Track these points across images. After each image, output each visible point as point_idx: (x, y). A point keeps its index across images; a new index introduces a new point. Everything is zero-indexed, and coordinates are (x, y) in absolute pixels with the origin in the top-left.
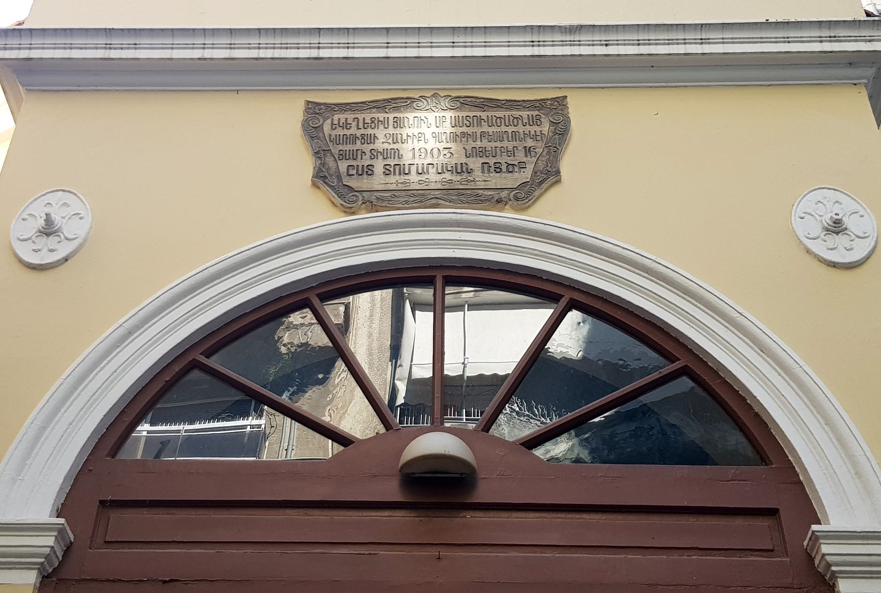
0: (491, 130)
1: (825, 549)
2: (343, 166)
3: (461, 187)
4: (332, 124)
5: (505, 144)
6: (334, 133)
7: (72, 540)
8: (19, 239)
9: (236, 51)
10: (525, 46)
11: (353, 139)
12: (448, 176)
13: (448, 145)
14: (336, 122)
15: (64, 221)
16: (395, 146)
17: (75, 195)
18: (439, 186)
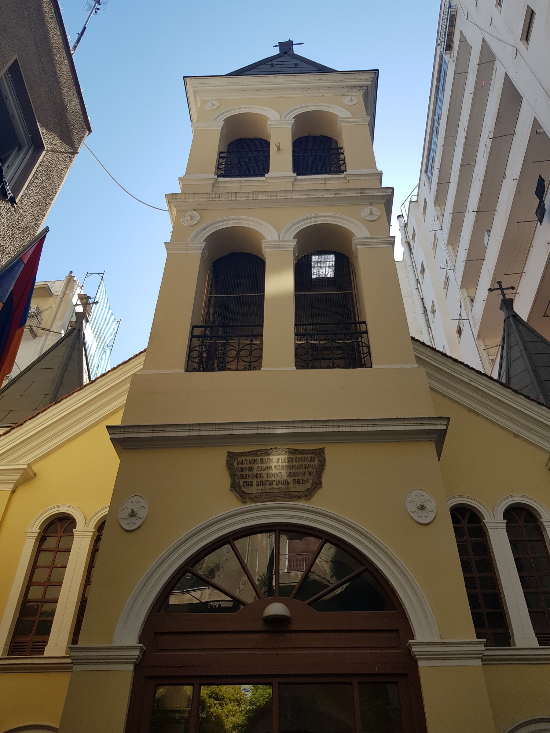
0: (296, 464)
1: (414, 649)
2: (241, 482)
3: (285, 491)
4: (237, 462)
5: (301, 470)
6: (238, 466)
7: (145, 650)
8: (122, 518)
9: (201, 432)
10: (309, 428)
11: (245, 469)
12: (280, 486)
13: (280, 472)
14: (239, 461)
15: (138, 509)
16: (260, 472)
17: (142, 497)
18: (277, 491)
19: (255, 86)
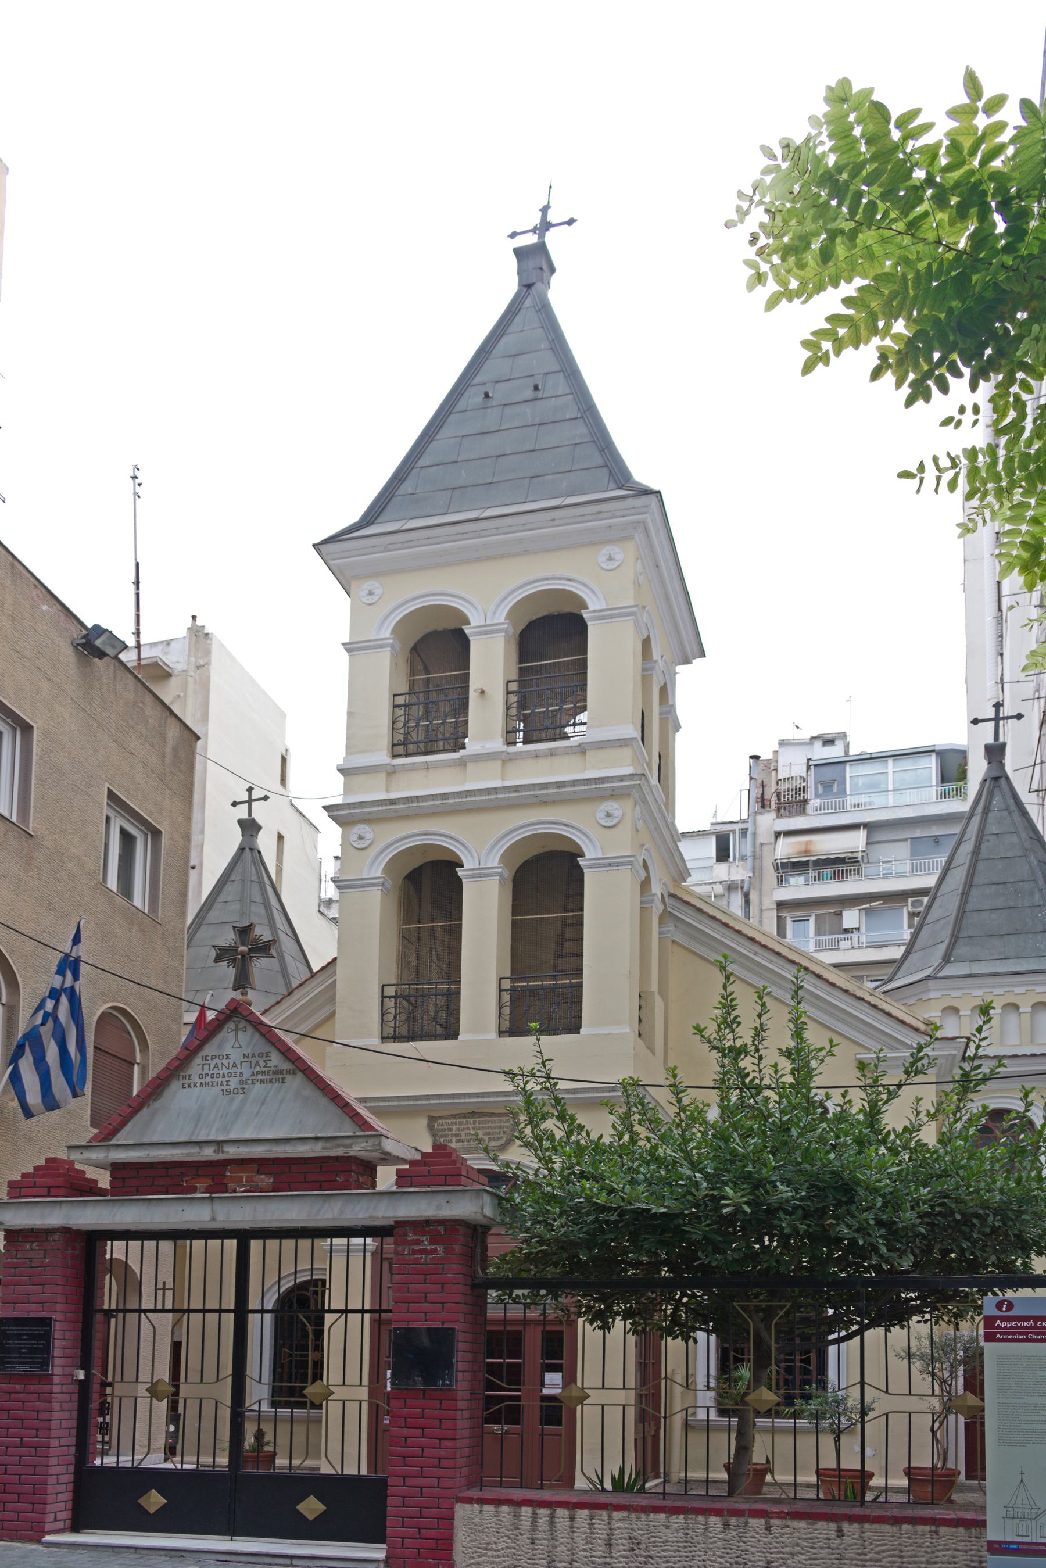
11: (445, 1130)
19: (544, 530)
